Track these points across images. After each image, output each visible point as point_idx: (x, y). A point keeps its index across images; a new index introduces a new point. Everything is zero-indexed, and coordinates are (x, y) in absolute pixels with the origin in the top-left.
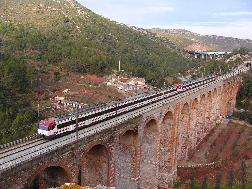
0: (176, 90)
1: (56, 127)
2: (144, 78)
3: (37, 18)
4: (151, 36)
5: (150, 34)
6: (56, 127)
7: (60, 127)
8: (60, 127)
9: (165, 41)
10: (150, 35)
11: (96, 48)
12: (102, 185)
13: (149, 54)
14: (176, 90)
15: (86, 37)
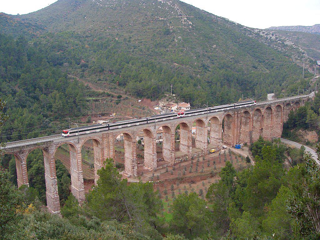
0: (177, 116)
1: (69, 133)
2: (189, 104)
3: (139, 31)
4: (279, 44)
5: (279, 40)
6: (69, 133)
7: (70, 133)
8: (70, 133)
9: (294, 49)
10: (279, 42)
11: (187, 65)
12: (86, 194)
13: (256, 68)
14: (177, 116)
15: (181, 52)
